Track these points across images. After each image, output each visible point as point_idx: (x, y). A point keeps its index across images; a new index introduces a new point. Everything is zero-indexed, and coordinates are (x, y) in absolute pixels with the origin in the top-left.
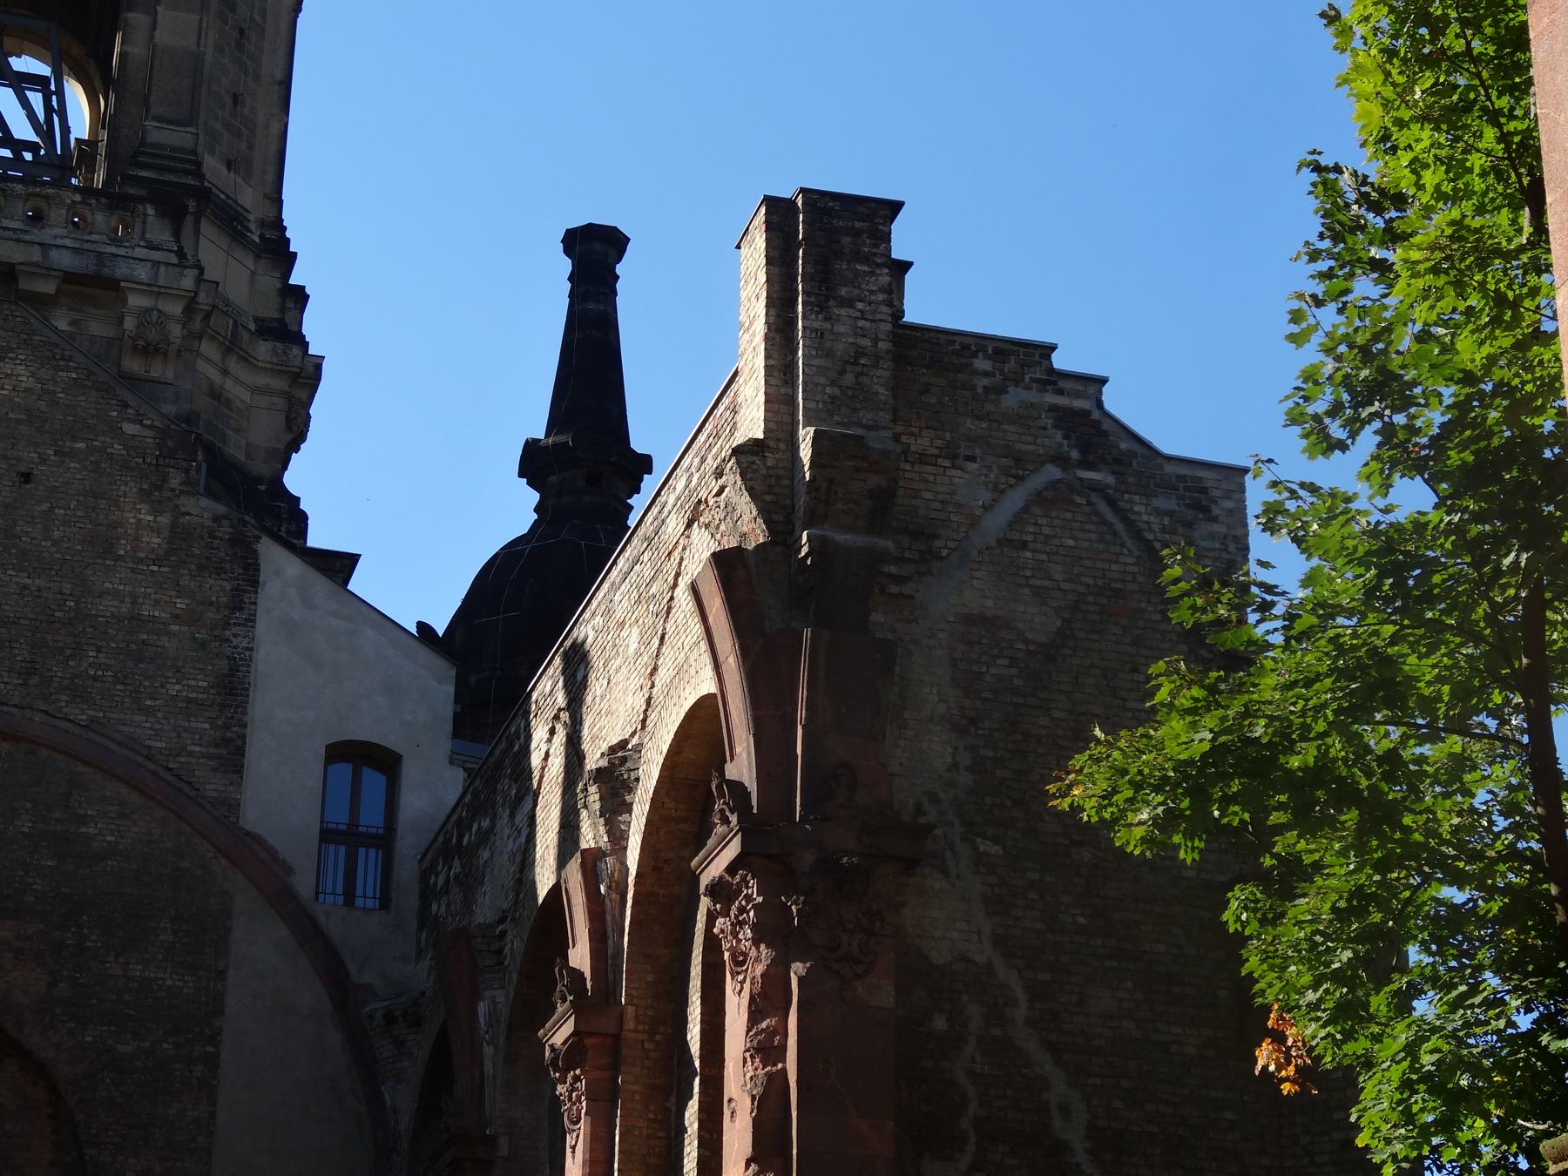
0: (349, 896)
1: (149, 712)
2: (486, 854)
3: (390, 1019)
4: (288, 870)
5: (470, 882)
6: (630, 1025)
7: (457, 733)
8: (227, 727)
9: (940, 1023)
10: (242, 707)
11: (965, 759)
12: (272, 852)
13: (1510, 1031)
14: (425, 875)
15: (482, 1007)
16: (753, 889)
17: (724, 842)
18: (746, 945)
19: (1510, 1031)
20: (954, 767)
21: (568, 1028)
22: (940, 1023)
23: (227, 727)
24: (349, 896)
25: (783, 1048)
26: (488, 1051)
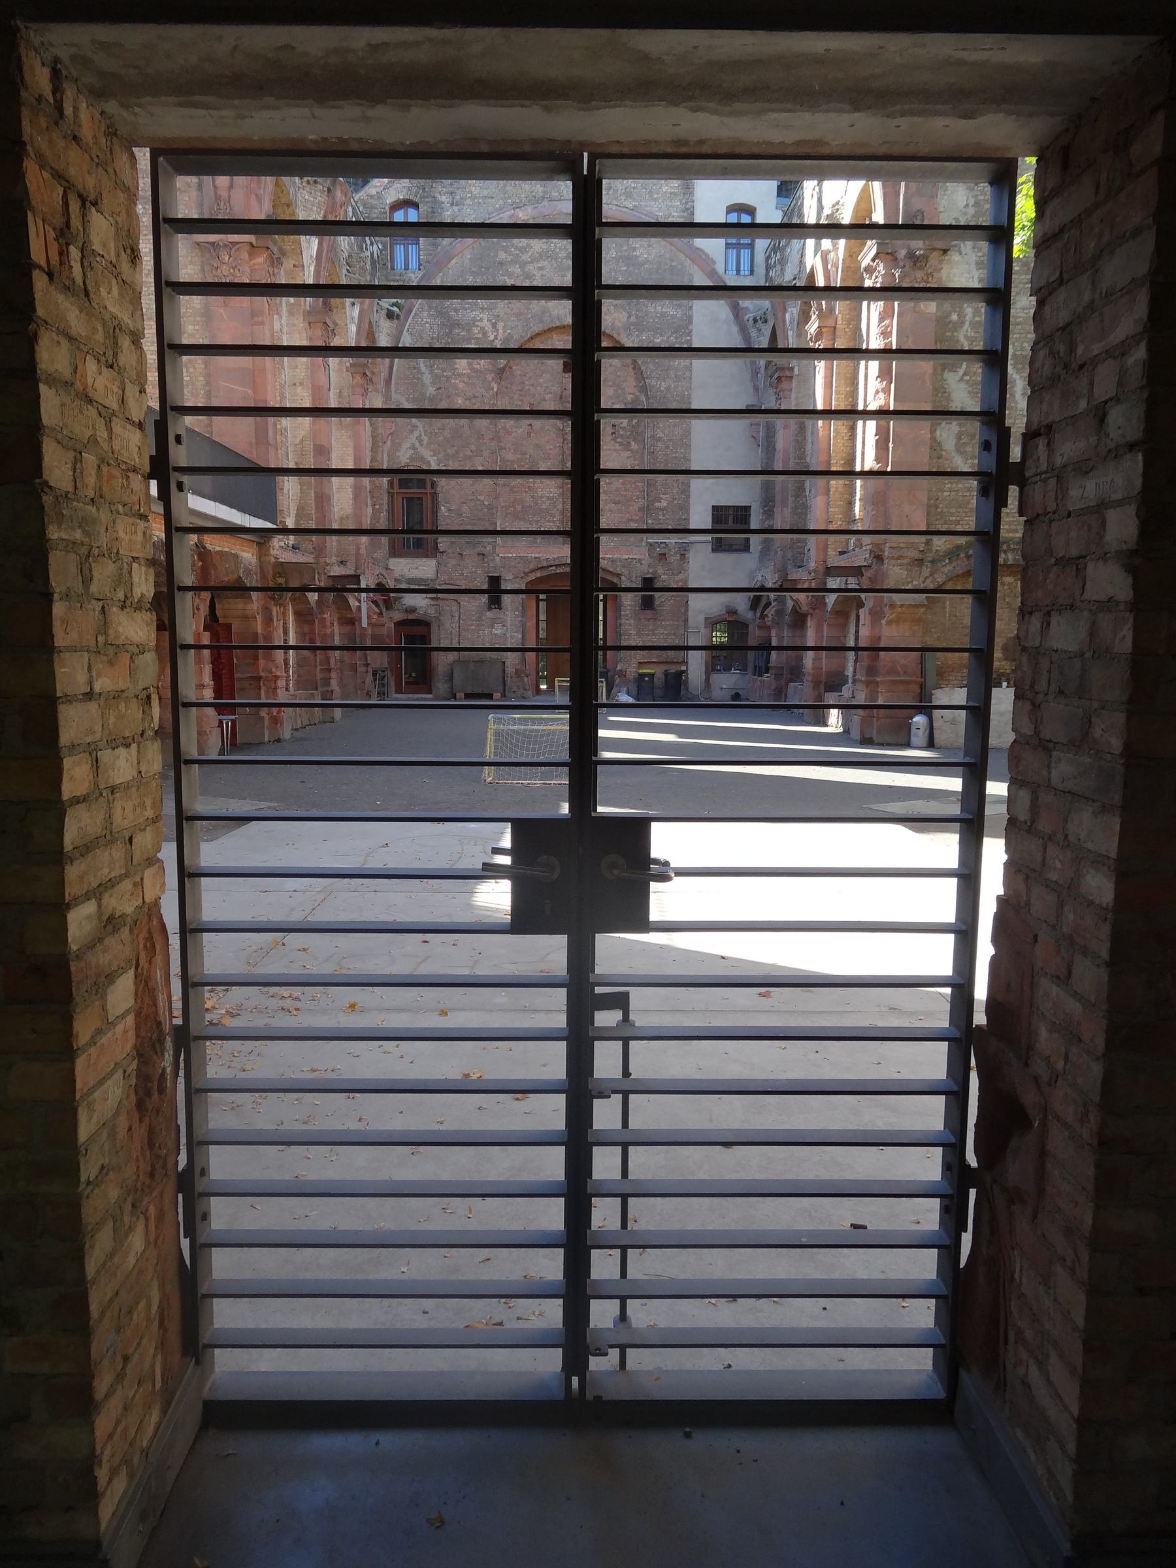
0: (738, 271)
1: (656, 200)
2: (788, 250)
3: (755, 321)
4: (714, 262)
5: (783, 262)
6: (839, 322)
7: (779, 195)
8: (686, 203)
9: (955, 317)
10: (692, 193)
11: (972, 202)
12: (707, 255)
13: (688, 1429)
14: (768, 258)
15: (787, 316)
16: (881, 267)
17: (871, 248)
18: (164, 1133)
19: (688, 1429)
20: (967, 205)
21: (816, 325)
22: (955, 317)
23: (686, 203)
24: (738, 271)
25: (891, 332)
26: (790, 333)
